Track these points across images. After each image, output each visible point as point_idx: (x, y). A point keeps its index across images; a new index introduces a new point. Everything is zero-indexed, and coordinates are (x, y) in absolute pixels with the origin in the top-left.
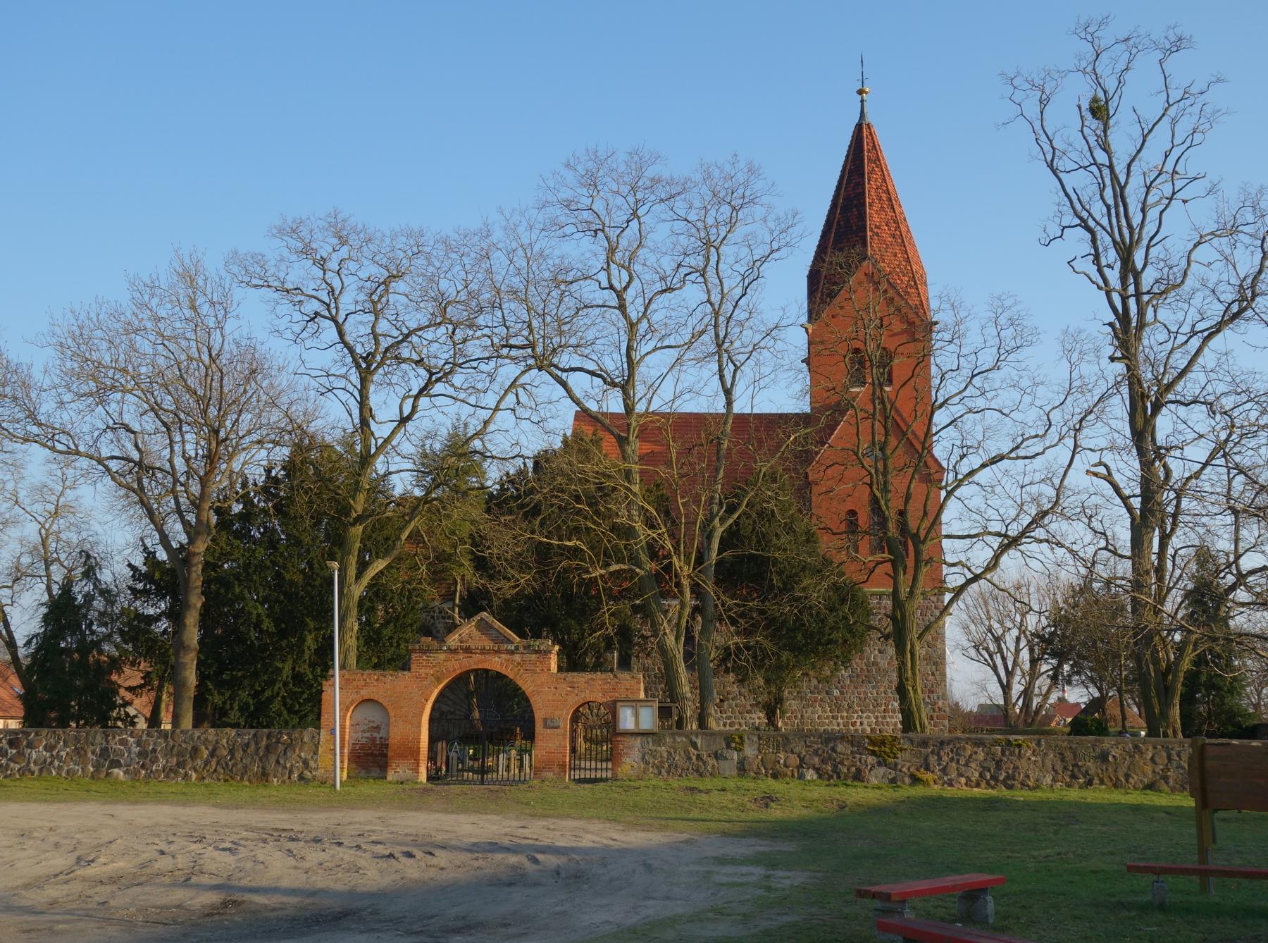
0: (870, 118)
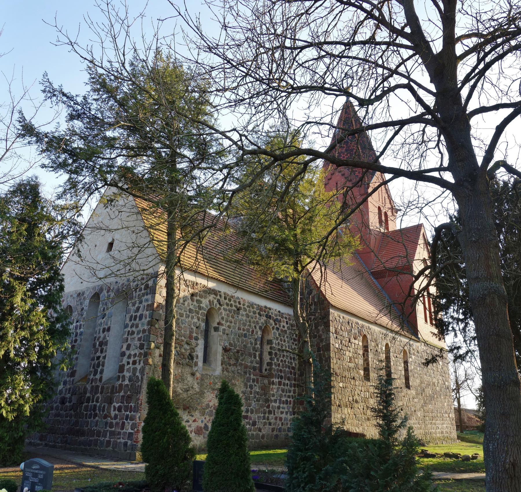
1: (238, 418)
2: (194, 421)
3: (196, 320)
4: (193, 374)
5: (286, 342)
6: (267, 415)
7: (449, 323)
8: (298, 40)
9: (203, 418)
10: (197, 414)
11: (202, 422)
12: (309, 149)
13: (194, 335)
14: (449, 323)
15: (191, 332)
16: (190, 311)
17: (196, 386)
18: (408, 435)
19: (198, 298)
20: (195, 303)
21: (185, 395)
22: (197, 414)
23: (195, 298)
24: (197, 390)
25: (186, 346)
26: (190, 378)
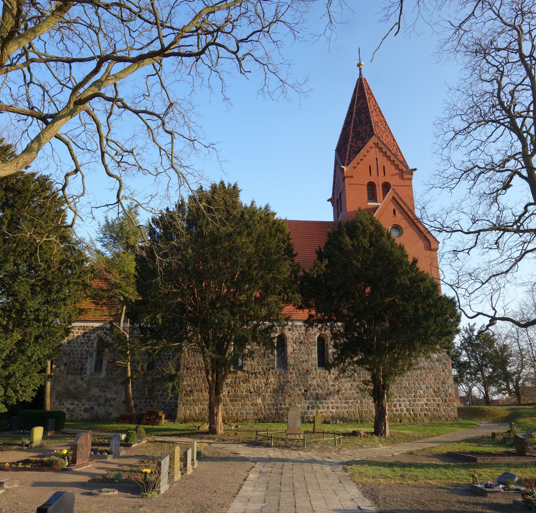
0: (364, 76)
1: (375, 401)
2: (83, 405)
3: (86, 348)
4: (82, 379)
5: (330, 407)
6: (149, 400)
7: (394, 300)
8: (198, 37)
9: (90, 403)
10: (84, 401)
11: (89, 405)
12: (141, 55)
13: (85, 356)
14: (394, 300)
15: (82, 354)
16: (82, 343)
17: (85, 386)
18: (369, 371)
19: (88, 335)
20: (86, 338)
21: (75, 391)
22: (84, 401)
23: (86, 335)
24: (85, 387)
25: (79, 364)
26: (80, 382)
